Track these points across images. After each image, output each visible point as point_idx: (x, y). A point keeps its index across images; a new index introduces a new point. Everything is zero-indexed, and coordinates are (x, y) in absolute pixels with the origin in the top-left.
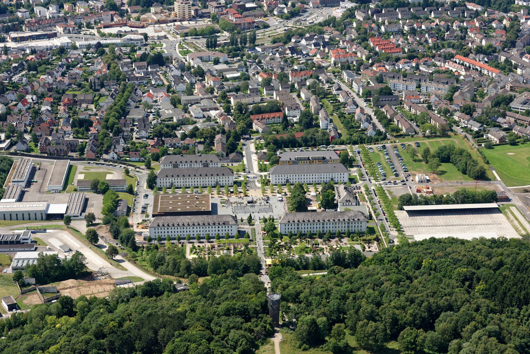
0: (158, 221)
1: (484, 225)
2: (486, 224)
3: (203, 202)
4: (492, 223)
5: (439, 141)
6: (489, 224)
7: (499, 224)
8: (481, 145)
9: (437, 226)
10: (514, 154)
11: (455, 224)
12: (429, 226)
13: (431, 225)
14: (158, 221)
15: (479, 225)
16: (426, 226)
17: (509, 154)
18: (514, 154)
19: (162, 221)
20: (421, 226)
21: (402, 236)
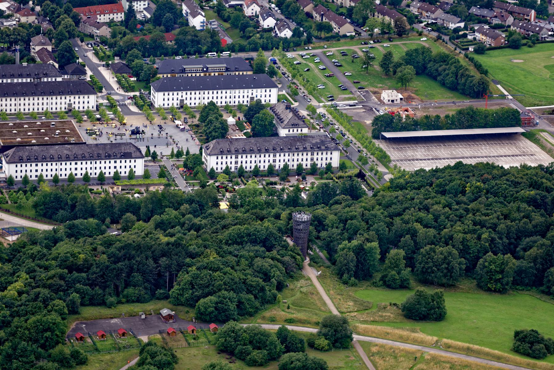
0: (20, 154)
1: (509, 156)
2: (513, 156)
3: (68, 131)
4: (520, 154)
5: (397, 45)
6: (517, 156)
7: (532, 155)
8: (468, 49)
9: (440, 159)
10: (522, 61)
11: (466, 155)
12: (429, 159)
13: (431, 158)
14: (20, 154)
15: (502, 156)
16: (425, 160)
17: (515, 61)
18: (522, 61)
19: (27, 154)
20: (417, 160)
21: (507, 34)
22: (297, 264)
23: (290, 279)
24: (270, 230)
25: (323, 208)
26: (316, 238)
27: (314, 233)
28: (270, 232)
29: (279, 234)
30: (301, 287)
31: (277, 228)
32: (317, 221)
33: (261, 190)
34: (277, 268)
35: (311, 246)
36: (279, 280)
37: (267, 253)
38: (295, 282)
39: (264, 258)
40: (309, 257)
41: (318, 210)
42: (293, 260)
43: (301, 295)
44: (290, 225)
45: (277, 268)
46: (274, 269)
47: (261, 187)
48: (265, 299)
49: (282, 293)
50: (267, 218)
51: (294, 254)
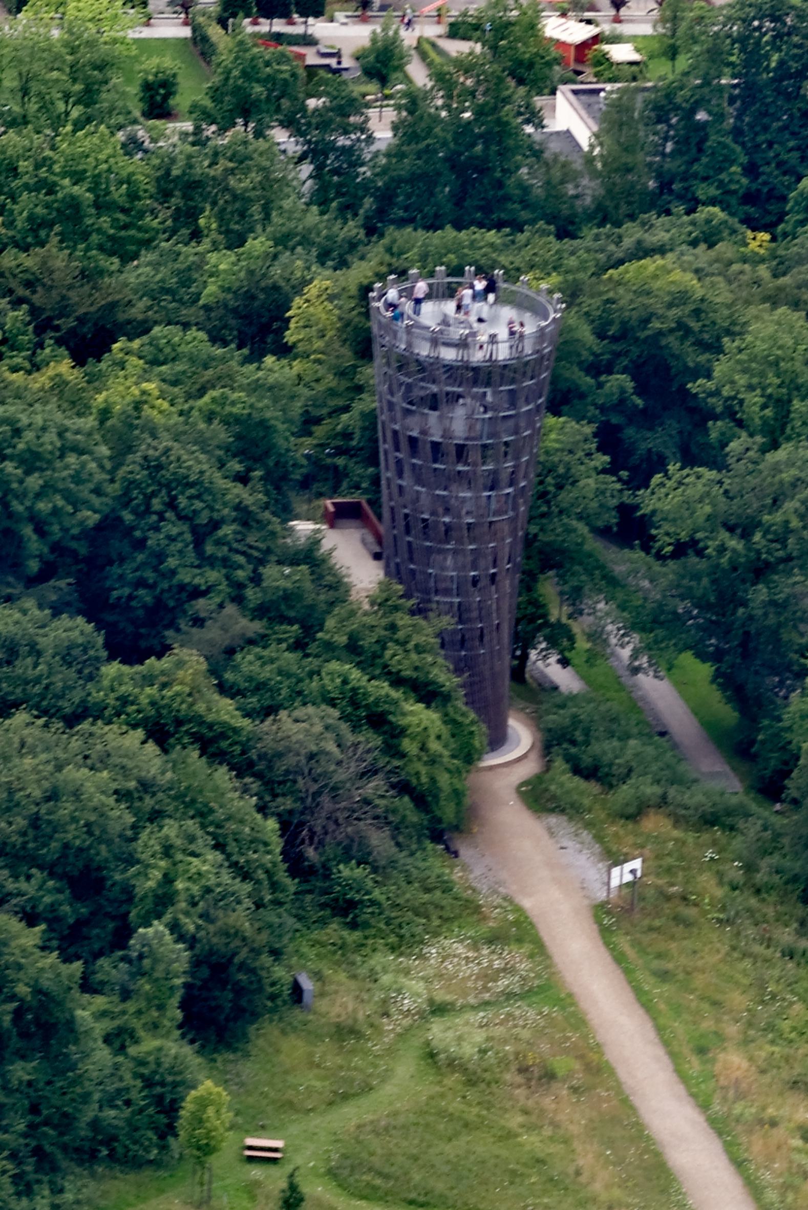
22: (403, 788)
23: (335, 931)
24: (146, 448)
25: (710, 238)
26: (604, 533)
27: (590, 483)
28: (154, 467)
29: (238, 491)
30: (439, 1009)
31: (221, 434)
32: (636, 371)
33: (168, 63)
34: (203, 814)
35: (557, 612)
36: (210, 935)
37: (112, 669)
38: (382, 959)
39: (72, 720)
40: (536, 720)
41: (651, 264)
42: (371, 739)
43: (426, 1089)
44: (365, 403)
45: (203, 814)
46: (170, 829)
47: (179, 31)
48: (65, 1122)
49: (247, 1069)
50: (142, 328)
51: (382, 688)
